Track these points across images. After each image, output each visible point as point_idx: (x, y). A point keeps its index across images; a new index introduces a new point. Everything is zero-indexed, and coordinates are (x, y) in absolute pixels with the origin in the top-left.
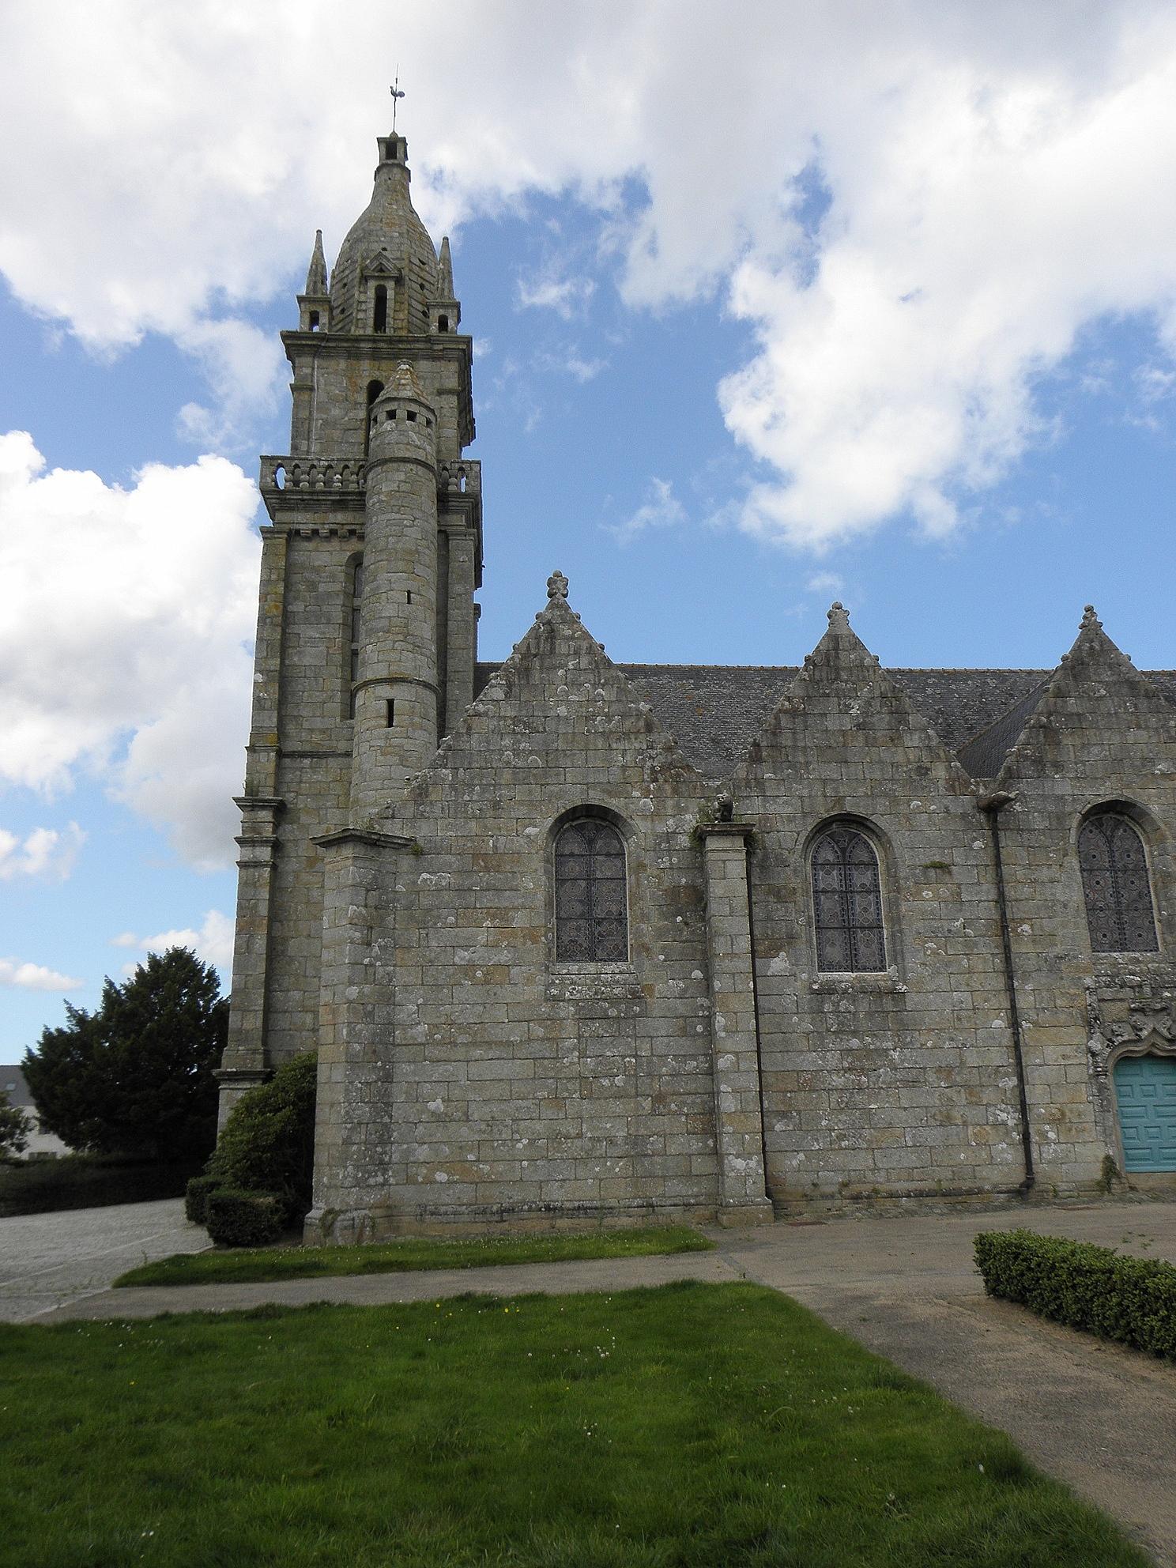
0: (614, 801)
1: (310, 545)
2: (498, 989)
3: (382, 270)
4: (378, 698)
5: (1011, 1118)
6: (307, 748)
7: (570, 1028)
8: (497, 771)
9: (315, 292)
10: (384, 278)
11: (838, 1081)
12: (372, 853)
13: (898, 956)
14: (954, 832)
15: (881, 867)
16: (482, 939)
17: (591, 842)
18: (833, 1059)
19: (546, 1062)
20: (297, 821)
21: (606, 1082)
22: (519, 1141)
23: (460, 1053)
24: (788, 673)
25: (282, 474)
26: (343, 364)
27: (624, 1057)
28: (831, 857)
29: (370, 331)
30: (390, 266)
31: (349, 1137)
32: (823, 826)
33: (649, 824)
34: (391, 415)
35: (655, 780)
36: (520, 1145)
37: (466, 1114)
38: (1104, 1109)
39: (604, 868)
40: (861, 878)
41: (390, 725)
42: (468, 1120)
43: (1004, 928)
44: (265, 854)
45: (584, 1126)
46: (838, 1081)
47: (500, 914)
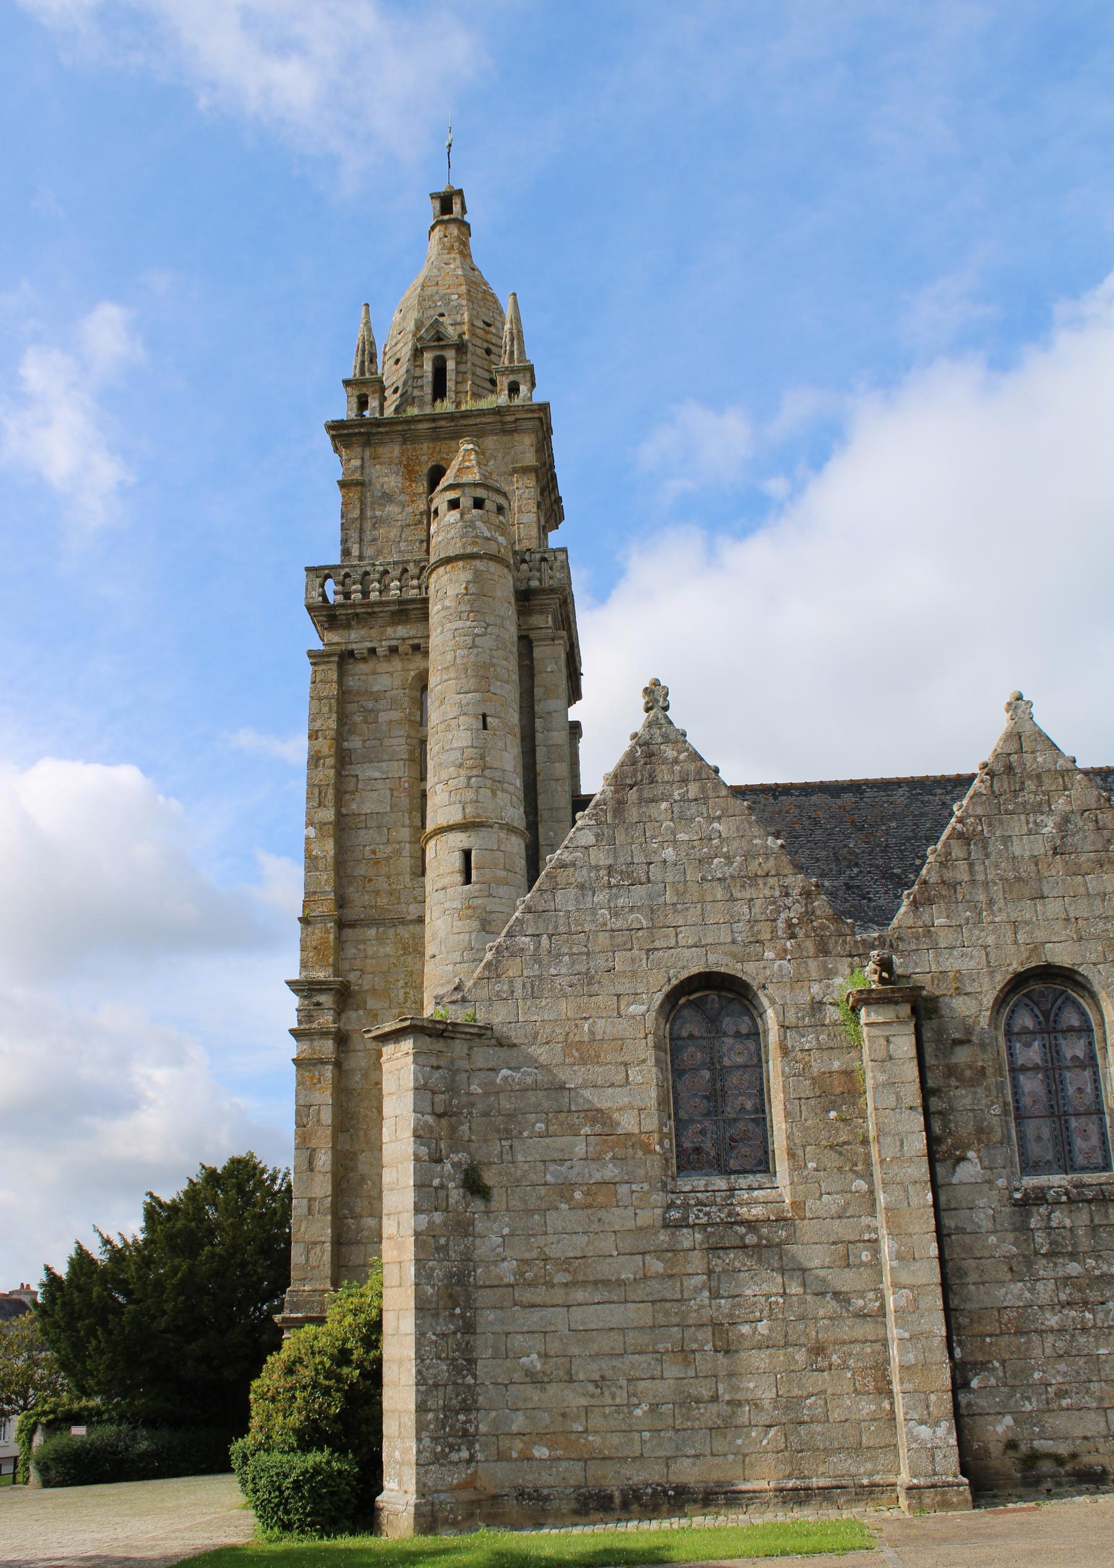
1: (363, 667)
2: (602, 1214)
3: (439, 339)
7: (697, 1262)
9: (362, 373)
10: (443, 347)
11: (1053, 1320)
12: (439, 1045)
16: (580, 1149)
18: (1045, 1291)
19: (668, 1305)
20: (362, 1006)
22: (637, 1406)
23: (558, 1295)
24: (962, 782)
25: (330, 586)
27: (768, 1296)
32: (1018, 982)
34: (454, 504)
35: (793, 936)
36: (638, 1412)
41: (468, 881)
42: (571, 1381)
44: (327, 1047)
46: (1053, 1320)
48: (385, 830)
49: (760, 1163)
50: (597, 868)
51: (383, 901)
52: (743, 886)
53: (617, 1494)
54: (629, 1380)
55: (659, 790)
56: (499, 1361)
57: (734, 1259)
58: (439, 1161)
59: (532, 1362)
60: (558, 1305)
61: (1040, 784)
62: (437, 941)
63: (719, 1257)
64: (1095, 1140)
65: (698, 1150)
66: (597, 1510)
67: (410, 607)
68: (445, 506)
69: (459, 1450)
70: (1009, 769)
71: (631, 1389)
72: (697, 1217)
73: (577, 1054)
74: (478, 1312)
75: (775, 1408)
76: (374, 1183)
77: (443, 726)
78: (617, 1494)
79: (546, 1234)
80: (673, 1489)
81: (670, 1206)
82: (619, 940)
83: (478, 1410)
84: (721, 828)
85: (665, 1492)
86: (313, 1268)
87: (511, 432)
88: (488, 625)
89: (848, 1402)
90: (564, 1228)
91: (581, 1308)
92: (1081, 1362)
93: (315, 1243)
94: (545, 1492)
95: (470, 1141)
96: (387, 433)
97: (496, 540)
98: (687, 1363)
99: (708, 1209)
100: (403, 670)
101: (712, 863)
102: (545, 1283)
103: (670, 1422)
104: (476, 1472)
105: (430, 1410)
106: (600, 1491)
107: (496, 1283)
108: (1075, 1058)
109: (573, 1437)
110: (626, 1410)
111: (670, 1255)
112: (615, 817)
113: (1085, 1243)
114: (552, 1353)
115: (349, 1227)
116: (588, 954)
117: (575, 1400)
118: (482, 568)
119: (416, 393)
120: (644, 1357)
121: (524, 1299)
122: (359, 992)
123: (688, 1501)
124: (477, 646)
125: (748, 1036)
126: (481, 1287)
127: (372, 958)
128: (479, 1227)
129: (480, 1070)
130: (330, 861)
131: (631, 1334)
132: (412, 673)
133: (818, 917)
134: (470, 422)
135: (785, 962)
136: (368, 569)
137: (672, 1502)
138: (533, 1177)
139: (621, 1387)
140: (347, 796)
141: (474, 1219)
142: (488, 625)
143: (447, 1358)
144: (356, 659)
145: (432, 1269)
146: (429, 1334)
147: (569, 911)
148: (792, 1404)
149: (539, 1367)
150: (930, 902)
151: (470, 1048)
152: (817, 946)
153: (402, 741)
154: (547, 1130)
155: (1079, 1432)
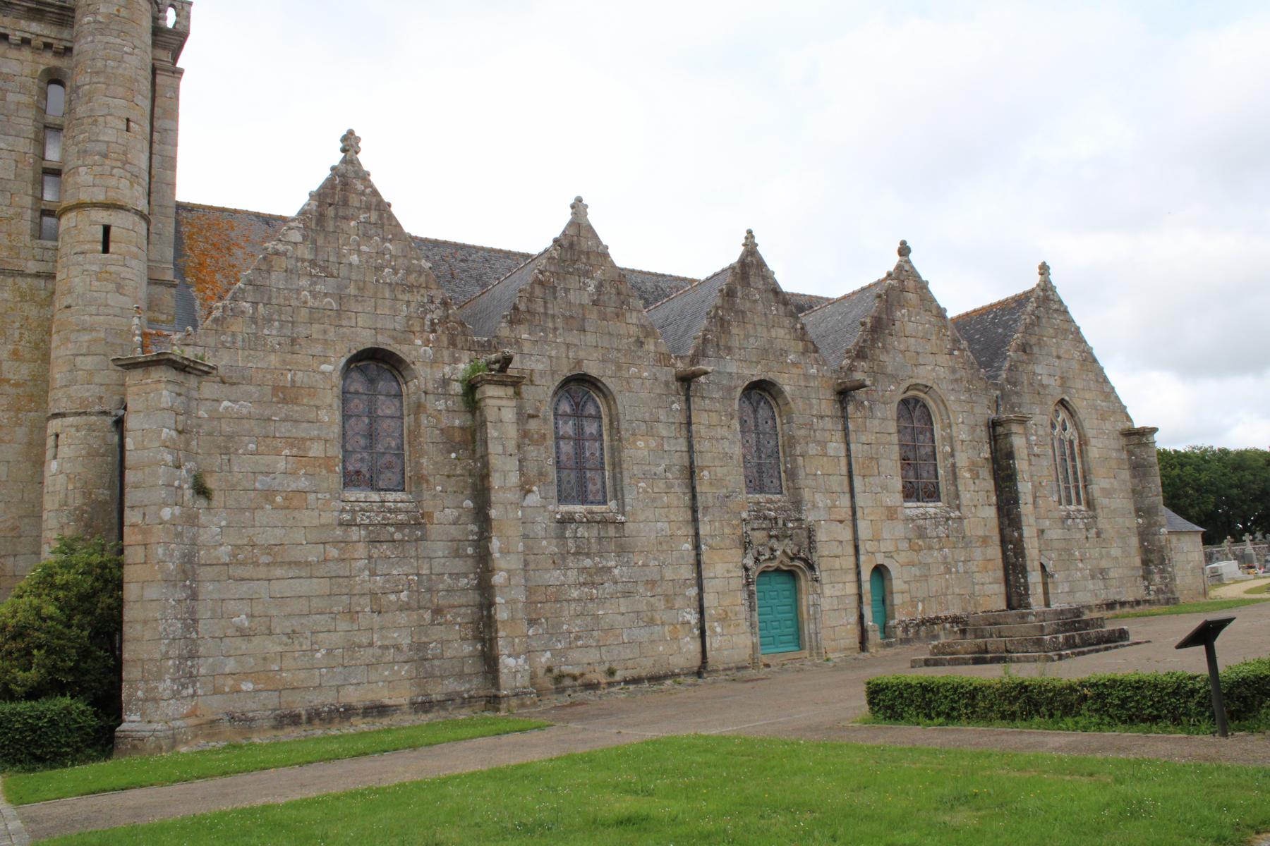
0: (398, 347)
2: (296, 514)
4: (96, 223)
5: (693, 618)
7: (361, 550)
8: (295, 310)
11: (575, 594)
13: (618, 494)
14: (660, 395)
15: (605, 420)
16: (281, 465)
17: (372, 381)
18: (572, 576)
21: (393, 597)
22: (317, 651)
27: (407, 575)
28: (568, 410)
31: (167, 652)
32: (567, 382)
33: (429, 370)
35: (434, 331)
36: (319, 655)
37: (269, 628)
38: (752, 608)
39: (386, 408)
40: (591, 428)
41: (106, 250)
42: (270, 634)
43: (692, 473)
45: (375, 637)
46: (575, 594)
47: (298, 443)
50: (303, 260)
53: (303, 713)
55: (350, 212)
58: (179, 467)
61: (588, 258)
64: (599, 485)
65: (358, 472)
70: (571, 245)
78: (303, 713)
79: (253, 526)
81: (343, 511)
85: (338, 710)
92: (589, 619)
94: (251, 715)
98: (353, 620)
103: (341, 661)
108: (591, 434)
109: (271, 674)
113: (595, 548)
116: (293, 323)
117: (273, 647)
120: (322, 617)
123: (353, 715)
125: (395, 396)
128: (203, 519)
131: (315, 600)
132: (42, 67)
148: (421, 647)
150: (520, 322)
151: (200, 383)
153: (31, 122)
155: (585, 661)
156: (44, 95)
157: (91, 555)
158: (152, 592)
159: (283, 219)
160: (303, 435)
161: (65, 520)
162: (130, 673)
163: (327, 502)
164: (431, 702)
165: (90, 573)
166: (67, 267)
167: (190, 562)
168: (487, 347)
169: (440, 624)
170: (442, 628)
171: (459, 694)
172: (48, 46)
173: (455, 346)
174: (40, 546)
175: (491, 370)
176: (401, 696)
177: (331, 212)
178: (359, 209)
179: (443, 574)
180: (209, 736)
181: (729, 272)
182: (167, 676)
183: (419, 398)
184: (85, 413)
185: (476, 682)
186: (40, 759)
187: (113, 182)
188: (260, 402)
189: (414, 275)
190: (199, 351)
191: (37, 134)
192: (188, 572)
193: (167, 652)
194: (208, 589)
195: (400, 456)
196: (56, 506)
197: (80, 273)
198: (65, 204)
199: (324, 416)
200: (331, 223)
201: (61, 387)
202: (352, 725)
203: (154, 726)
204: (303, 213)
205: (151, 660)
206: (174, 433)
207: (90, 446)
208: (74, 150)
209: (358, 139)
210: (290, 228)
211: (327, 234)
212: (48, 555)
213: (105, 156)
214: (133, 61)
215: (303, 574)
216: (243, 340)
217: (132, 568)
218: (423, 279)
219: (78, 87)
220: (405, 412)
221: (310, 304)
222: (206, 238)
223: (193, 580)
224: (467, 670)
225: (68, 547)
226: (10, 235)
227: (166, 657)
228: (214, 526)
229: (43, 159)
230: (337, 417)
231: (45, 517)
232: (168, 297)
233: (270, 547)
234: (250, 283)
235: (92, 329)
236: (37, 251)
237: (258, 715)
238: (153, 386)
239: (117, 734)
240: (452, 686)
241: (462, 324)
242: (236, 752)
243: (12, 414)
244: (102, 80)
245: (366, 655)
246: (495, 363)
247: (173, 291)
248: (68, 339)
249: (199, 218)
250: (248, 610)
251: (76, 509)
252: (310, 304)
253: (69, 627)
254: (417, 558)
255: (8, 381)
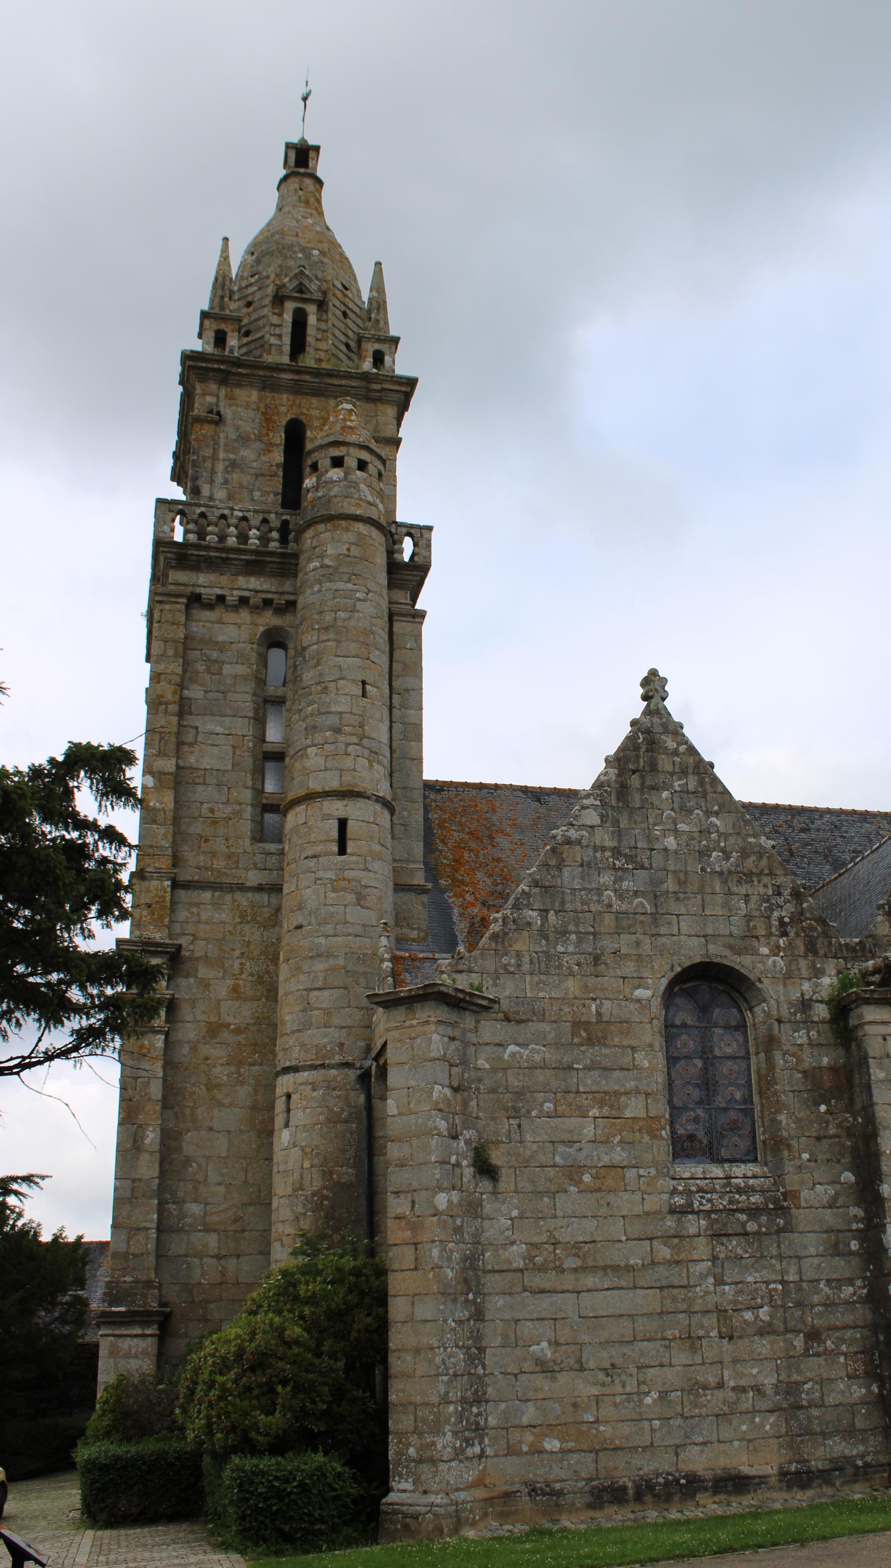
1: (207, 615)
2: (611, 1198)
4: (326, 817)
6: (209, 876)
7: (701, 1248)
9: (222, 308)
16: (589, 1131)
19: (675, 1291)
21: (748, 1316)
22: (647, 1394)
23: (568, 1280)
26: (254, 395)
27: (767, 1283)
29: (286, 359)
30: (313, 287)
31: (447, 1393)
33: (781, 988)
35: (784, 934)
36: (648, 1400)
37: (579, 1361)
39: (725, 1045)
41: (342, 851)
42: (582, 1369)
45: (726, 1373)
48: (226, 789)
49: (748, 1152)
50: (603, 849)
51: (219, 863)
52: (738, 881)
53: (630, 1485)
54: (638, 1367)
55: (662, 778)
56: (509, 1350)
57: (737, 1245)
59: (542, 1350)
60: (568, 1291)
62: (306, 912)
63: (722, 1244)
65: (691, 1137)
66: (611, 1502)
67: (269, 559)
68: (328, 462)
69: (473, 1445)
71: (641, 1376)
72: (701, 1204)
73: (584, 1034)
74: (487, 1298)
75: (777, 1393)
76: (200, 1166)
77: (319, 688)
78: (630, 1485)
79: (555, 1217)
80: (684, 1477)
81: (674, 1192)
82: (625, 923)
83: (487, 1402)
84: (718, 823)
85: (677, 1481)
86: (135, 1256)
87: (375, 401)
88: (369, 591)
89: (842, 1386)
90: (573, 1212)
91: (591, 1294)
93: (139, 1229)
94: (558, 1486)
95: (478, 1118)
96: (247, 375)
97: (376, 506)
98: (694, 1349)
99: (709, 1196)
100: (252, 624)
101: (710, 856)
102: (555, 1268)
104: (485, 1467)
105: (452, 1402)
106: (612, 1483)
107: (505, 1267)
109: (584, 1427)
110: (636, 1398)
111: (676, 1241)
112: (618, 800)
114: (562, 1341)
115: (170, 1213)
116: (594, 934)
118: (365, 532)
119: (273, 340)
121: (534, 1285)
122: (190, 959)
124: (358, 611)
126: (490, 1271)
127: (206, 923)
128: (488, 1208)
129: (487, 1044)
130: (170, 815)
132: (262, 629)
133: (807, 919)
134: (336, 382)
135: (778, 959)
136: (226, 512)
137: (684, 1490)
138: (543, 1159)
139: (631, 1375)
140: (186, 748)
141: (482, 1200)
142: (369, 591)
143: (463, 1347)
144: (227, 606)
145: (451, 1251)
146: (450, 1321)
147: (575, 889)
148: (790, 1389)
149: (549, 1355)
151: (478, 1022)
152: (806, 946)
153: (249, 697)
154: (556, 1110)
156: (263, 661)
157: (341, 1256)
158: (425, 1310)
159: (570, 795)
160: (616, 1087)
161: (300, 1209)
162: (399, 1422)
163: (652, 1182)
164: (809, 1472)
165: (342, 1282)
166: (297, 875)
167: (473, 1267)
168: (859, 952)
169: (817, 1355)
170: (821, 1360)
171: (850, 1460)
172: (268, 603)
173: (815, 953)
174: (269, 1244)
175: (869, 984)
176: (765, 1463)
177: (635, 781)
178: (672, 774)
179: (818, 1281)
180: (504, 1516)
181: (417, 722)
182: (447, 1428)
183: (770, 1028)
184: (323, 1066)
185: (874, 1441)
186: (288, 1538)
187: (348, 763)
188: (557, 1045)
189: (753, 858)
190: (475, 979)
191: (256, 710)
192: (471, 1282)
193: (447, 1393)
194: (496, 1305)
195: (748, 1112)
196: (289, 1191)
197: (310, 886)
198: (291, 795)
199: (642, 1060)
200: (637, 796)
201: (293, 1032)
202: (698, 1505)
203: (431, 1498)
204: (598, 785)
205: (427, 1404)
206: (447, 1091)
207: (330, 1109)
208: (300, 726)
209: (664, 681)
210: (584, 808)
211: (632, 812)
212: (282, 1256)
213: (338, 731)
214: (366, 608)
215: (624, 1284)
216: (531, 962)
217: (399, 1276)
218: (764, 862)
219: (304, 649)
220: (752, 1050)
221: (615, 907)
222: (461, 824)
223: (477, 1293)
224: (859, 1424)
225: (310, 1245)
226: (227, 840)
227: (445, 1400)
228: (501, 1217)
229: (264, 741)
230: (660, 1060)
231: (275, 1205)
232: (418, 906)
233: (577, 1245)
234: (536, 884)
235: (329, 955)
236: (259, 858)
237: (567, 1486)
238: (420, 1029)
239: (383, 1508)
240: (838, 1447)
241: (822, 921)
242: (546, 1540)
243: (233, 1069)
244: (332, 636)
245: (715, 1400)
246: (873, 973)
247: (425, 898)
248: (299, 969)
249: (450, 800)
250: (551, 1335)
251: (313, 1195)
252: (615, 907)
253: (318, 1355)
254: (780, 1257)
255: (227, 1026)
